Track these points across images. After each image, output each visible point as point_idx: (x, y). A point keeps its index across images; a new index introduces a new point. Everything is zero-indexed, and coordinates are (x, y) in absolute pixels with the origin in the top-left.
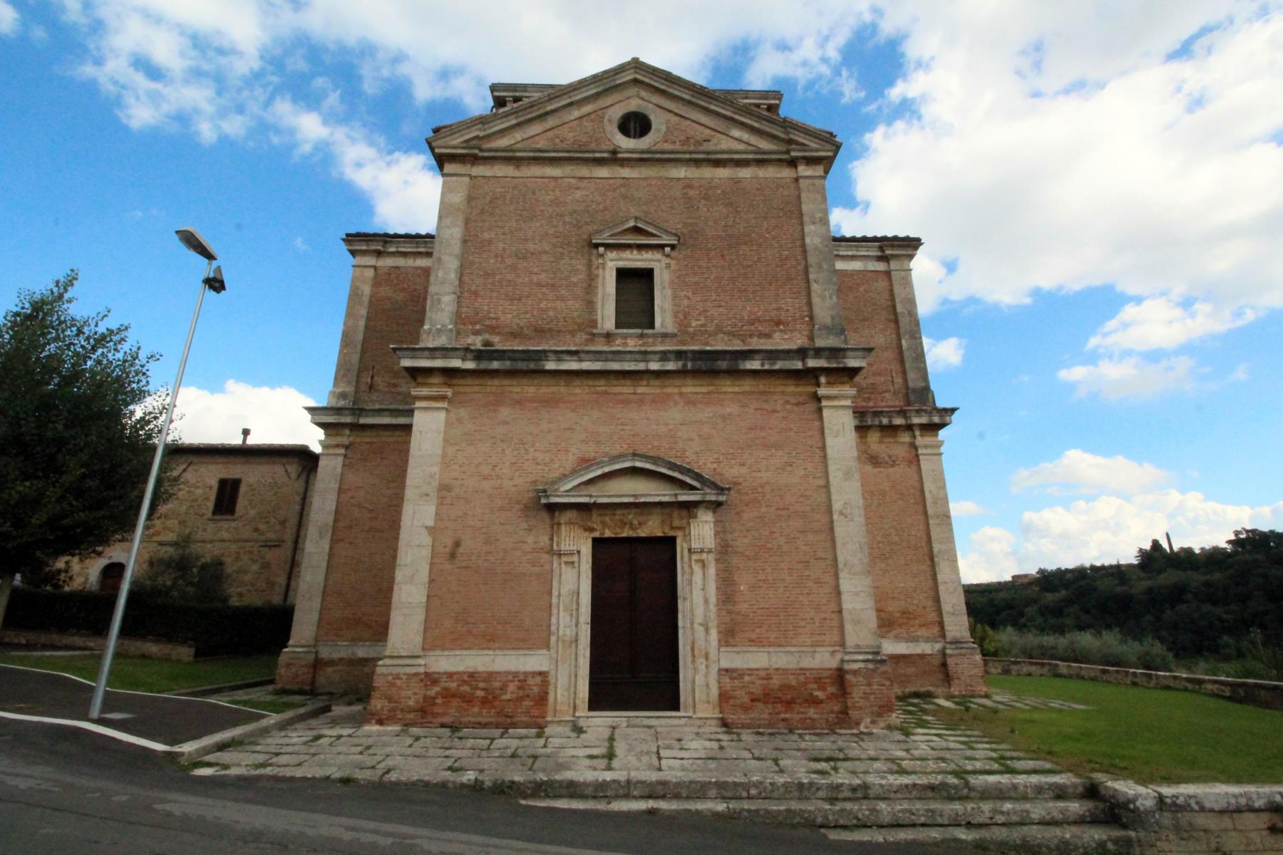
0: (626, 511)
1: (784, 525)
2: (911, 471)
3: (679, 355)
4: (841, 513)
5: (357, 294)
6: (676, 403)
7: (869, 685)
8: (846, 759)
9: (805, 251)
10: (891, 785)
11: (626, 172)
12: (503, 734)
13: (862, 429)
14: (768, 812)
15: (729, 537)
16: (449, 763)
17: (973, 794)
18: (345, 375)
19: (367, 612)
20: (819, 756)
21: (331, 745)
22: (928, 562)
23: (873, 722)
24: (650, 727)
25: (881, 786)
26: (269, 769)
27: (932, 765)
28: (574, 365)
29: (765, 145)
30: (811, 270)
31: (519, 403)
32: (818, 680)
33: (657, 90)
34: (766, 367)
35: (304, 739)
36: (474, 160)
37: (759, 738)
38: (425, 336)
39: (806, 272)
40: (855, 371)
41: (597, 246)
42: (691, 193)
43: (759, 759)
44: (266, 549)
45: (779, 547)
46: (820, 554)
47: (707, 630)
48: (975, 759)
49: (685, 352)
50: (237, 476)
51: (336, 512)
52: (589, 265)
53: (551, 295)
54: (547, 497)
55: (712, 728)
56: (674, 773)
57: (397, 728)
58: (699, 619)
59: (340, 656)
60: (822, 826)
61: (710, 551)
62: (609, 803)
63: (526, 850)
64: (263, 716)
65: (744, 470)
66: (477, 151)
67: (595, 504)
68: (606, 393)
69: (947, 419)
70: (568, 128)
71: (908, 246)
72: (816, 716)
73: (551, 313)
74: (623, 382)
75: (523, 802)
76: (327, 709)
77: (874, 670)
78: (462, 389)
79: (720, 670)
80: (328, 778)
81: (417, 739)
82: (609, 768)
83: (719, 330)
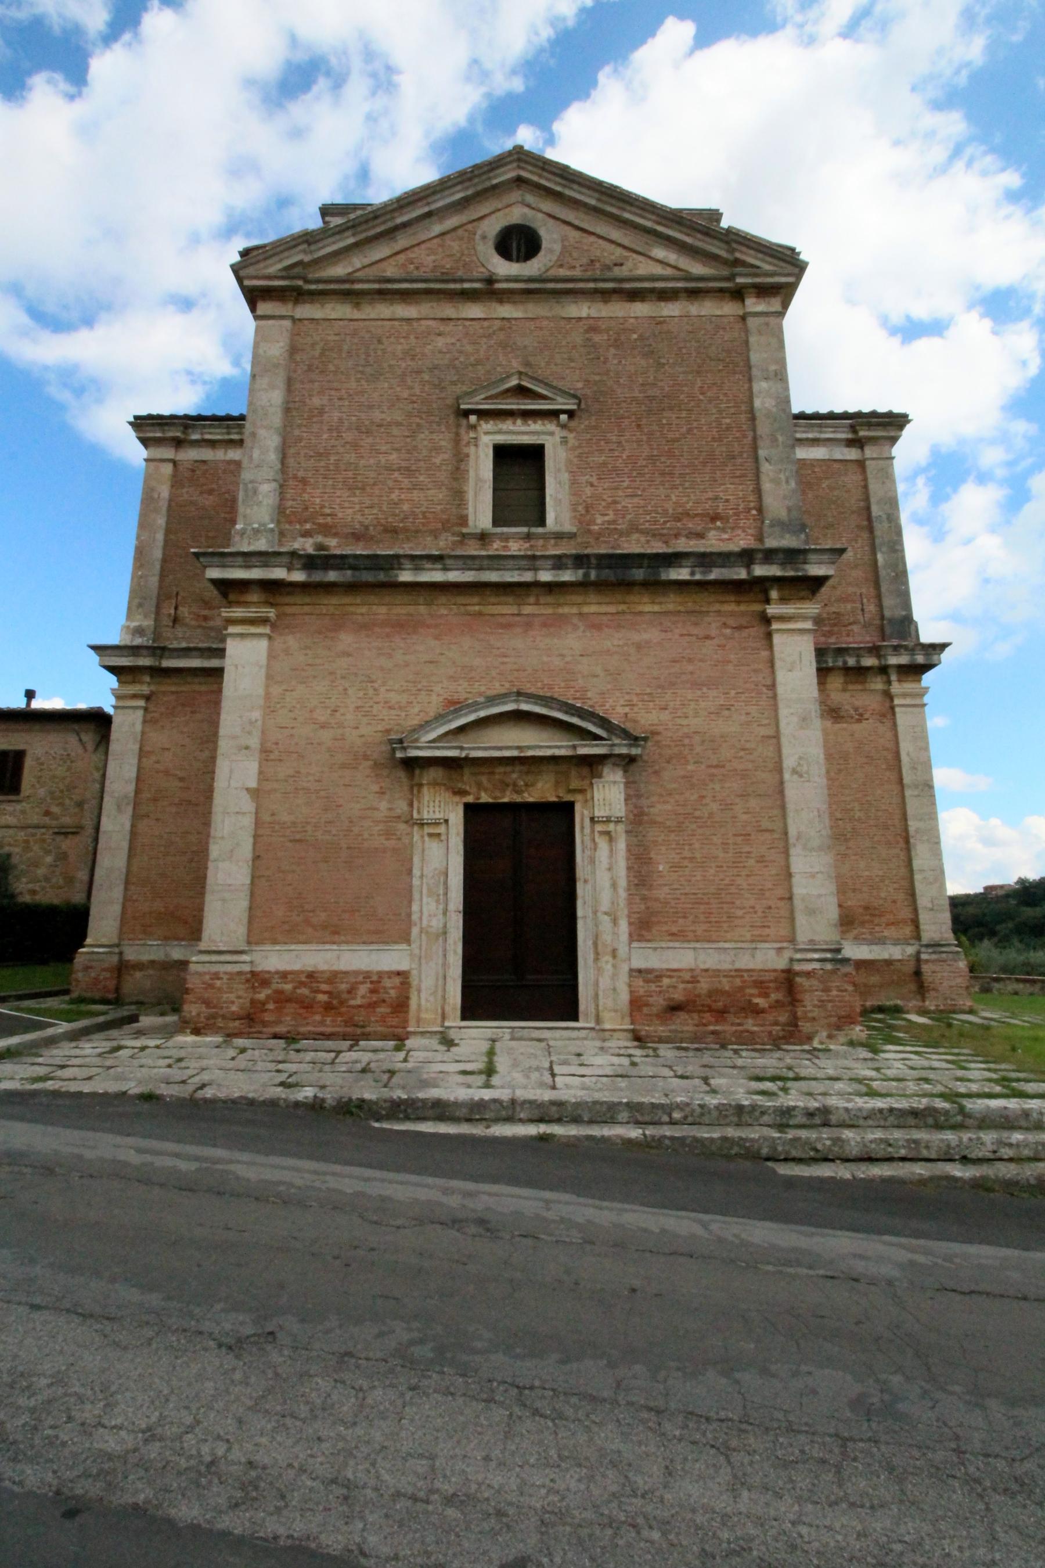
0: (509, 769)
1: (717, 787)
2: (884, 729)
3: (580, 561)
4: (794, 772)
5: (152, 498)
6: (575, 628)
7: (826, 990)
8: (797, 1079)
9: (753, 419)
10: (860, 1110)
11: (506, 311)
12: (352, 1046)
13: (823, 672)
14: (696, 1139)
15: (644, 802)
16: (282, 1077)
17: (969, 1122)
18: (140, 605)
19: (175, 902)
20: (761, 1074)
21: (131, 1057)
22: (902, 845)
23: (830, 1037)
24: (540, 1040)
25: (847, 1110)
26: (50, 1082)
27: (912, 1087)
28: (437, 576)
29: (697, 269)
30: (760, 443)
31: (365, 627)
32: (759, 984)
33: (549, 193)
34: (698, 577)
35: (99, 1050)
36: (299, 295)
37: (683, 1054)
38: (237, 538)
39: (755, 448)
40: (819, 582)
41: (467, 413)
42: (597, 338)
43: (682, 1077)
44: (62, 837)
45: (711, 815)
46: (766, 824)
47: (615, 921)
48: (969, 1080)
49: (588, 556)
50: (21, 747)
51: (138, 779)
52: (457, 441)
53: (406, 482)
54: (404, 749)
55: (623, 1042)
56: (572, 1092)
57: (218, 1039)
58: (605, 905)
59: (152, 957)
60: (768, 1159)
61: (618, 821)
62: (488, 1127)
63: (375, 1179)
64: (52, 1025)
65: (665, 716)
66: (300, 283)
67: (467, 759)
68: (480, 614)
69: (935, 657)
70: (425, 253)
71: (890, 424)
72: (755, 1029)
73: (406, 507)
74: (503, 599)
75: (377, 1125)
76: (133, 1019)
77: (834, 972)
78: (288, 610)
79: (631, 970)
80: (125, 1093)
81: (243, 1051)
82: (487, 1085)
83: (634, 528)
